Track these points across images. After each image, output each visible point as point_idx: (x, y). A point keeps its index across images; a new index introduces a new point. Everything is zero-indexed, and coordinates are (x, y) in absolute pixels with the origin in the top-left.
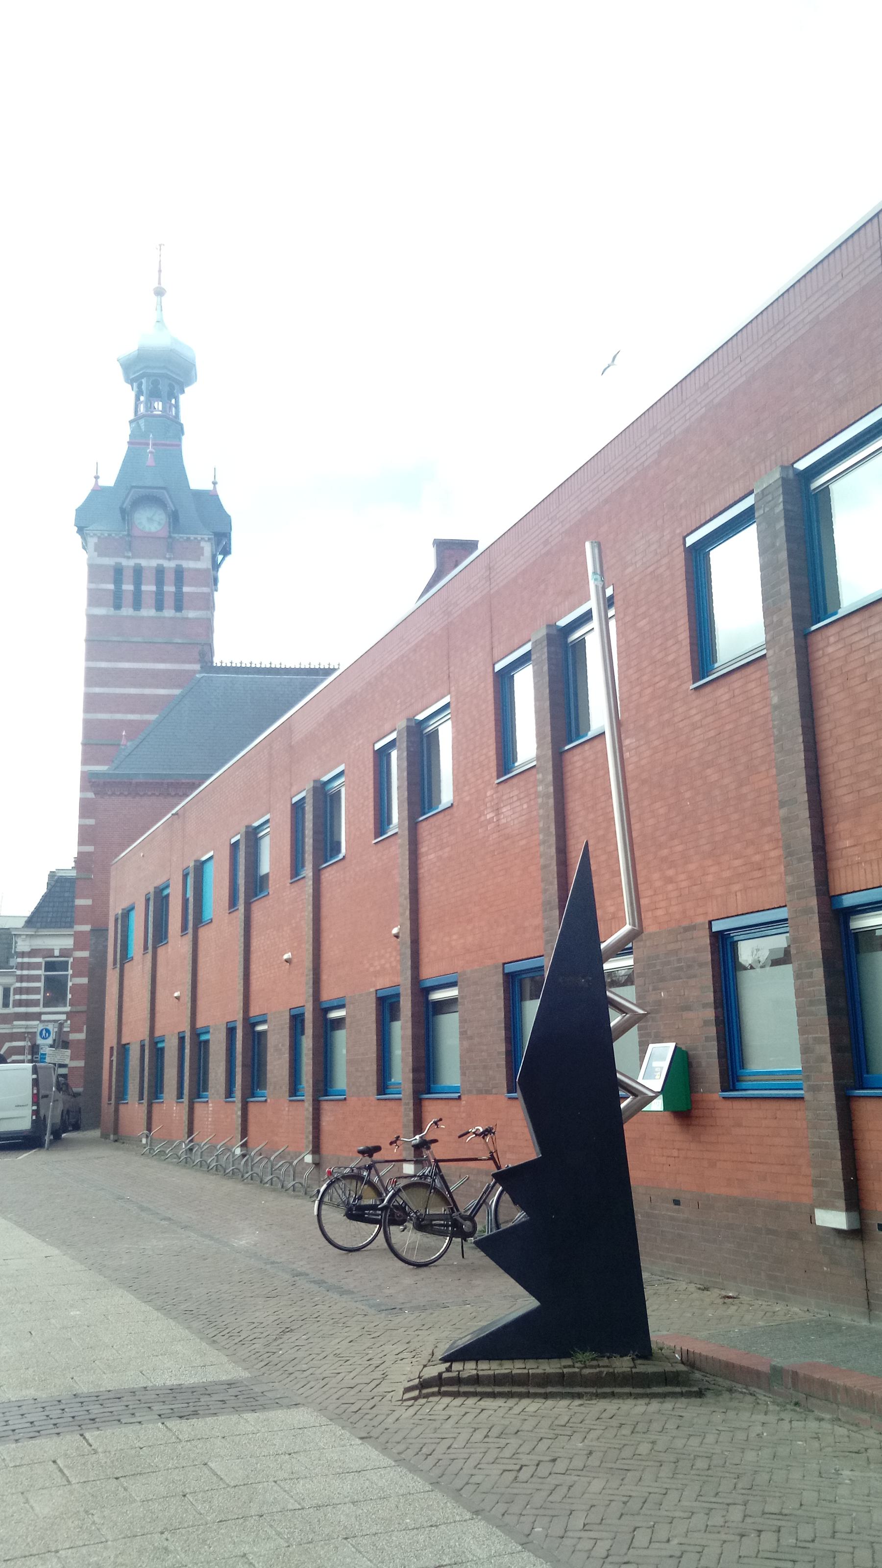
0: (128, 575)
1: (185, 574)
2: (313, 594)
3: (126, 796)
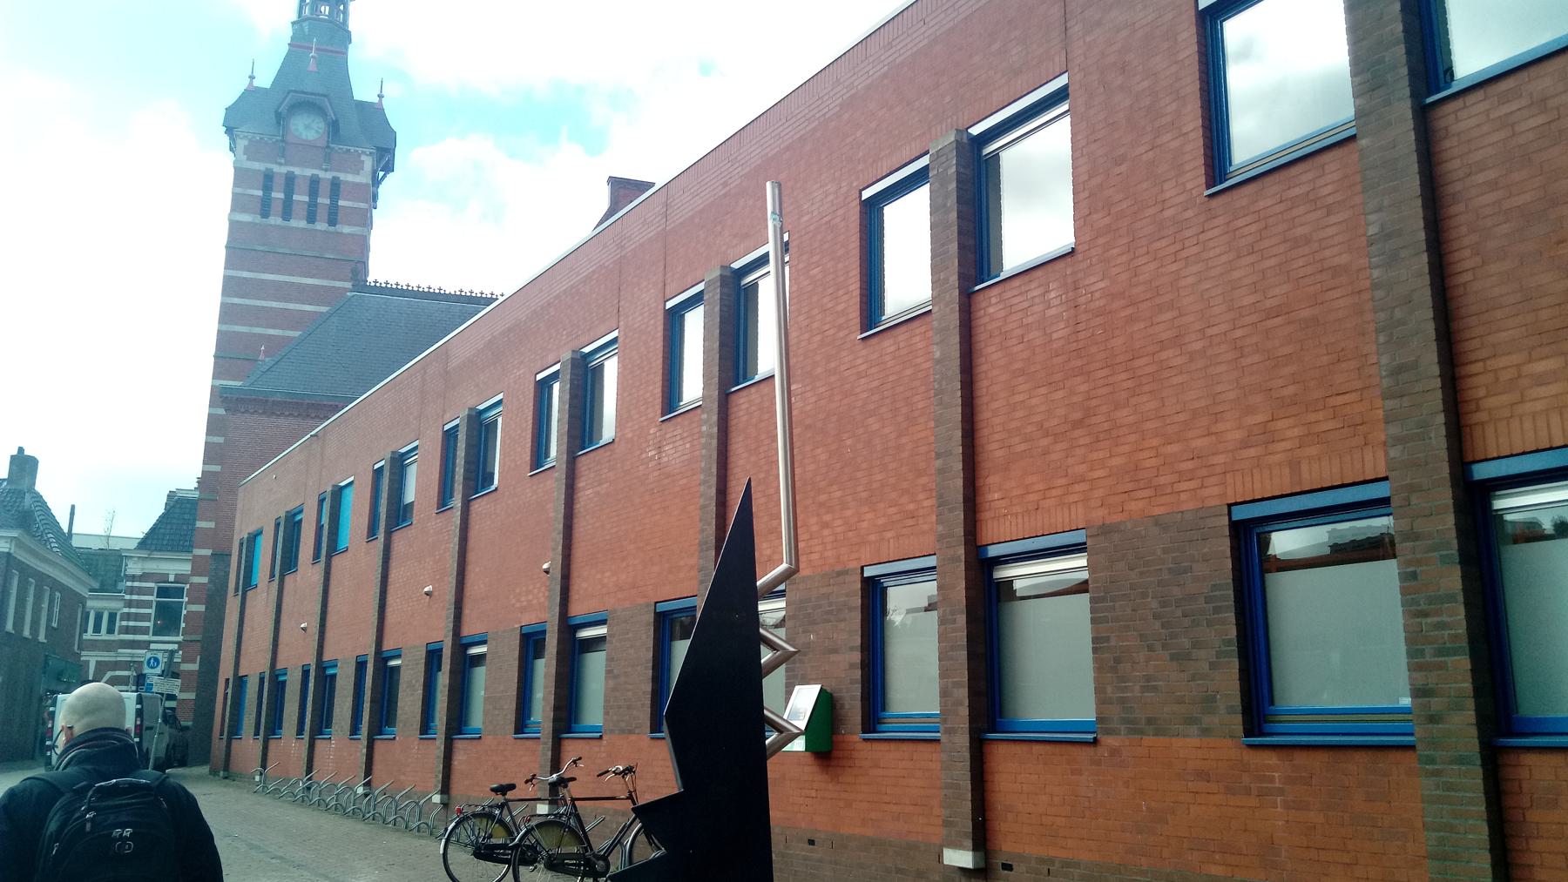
0: (279, 182)
2: (469, 224)
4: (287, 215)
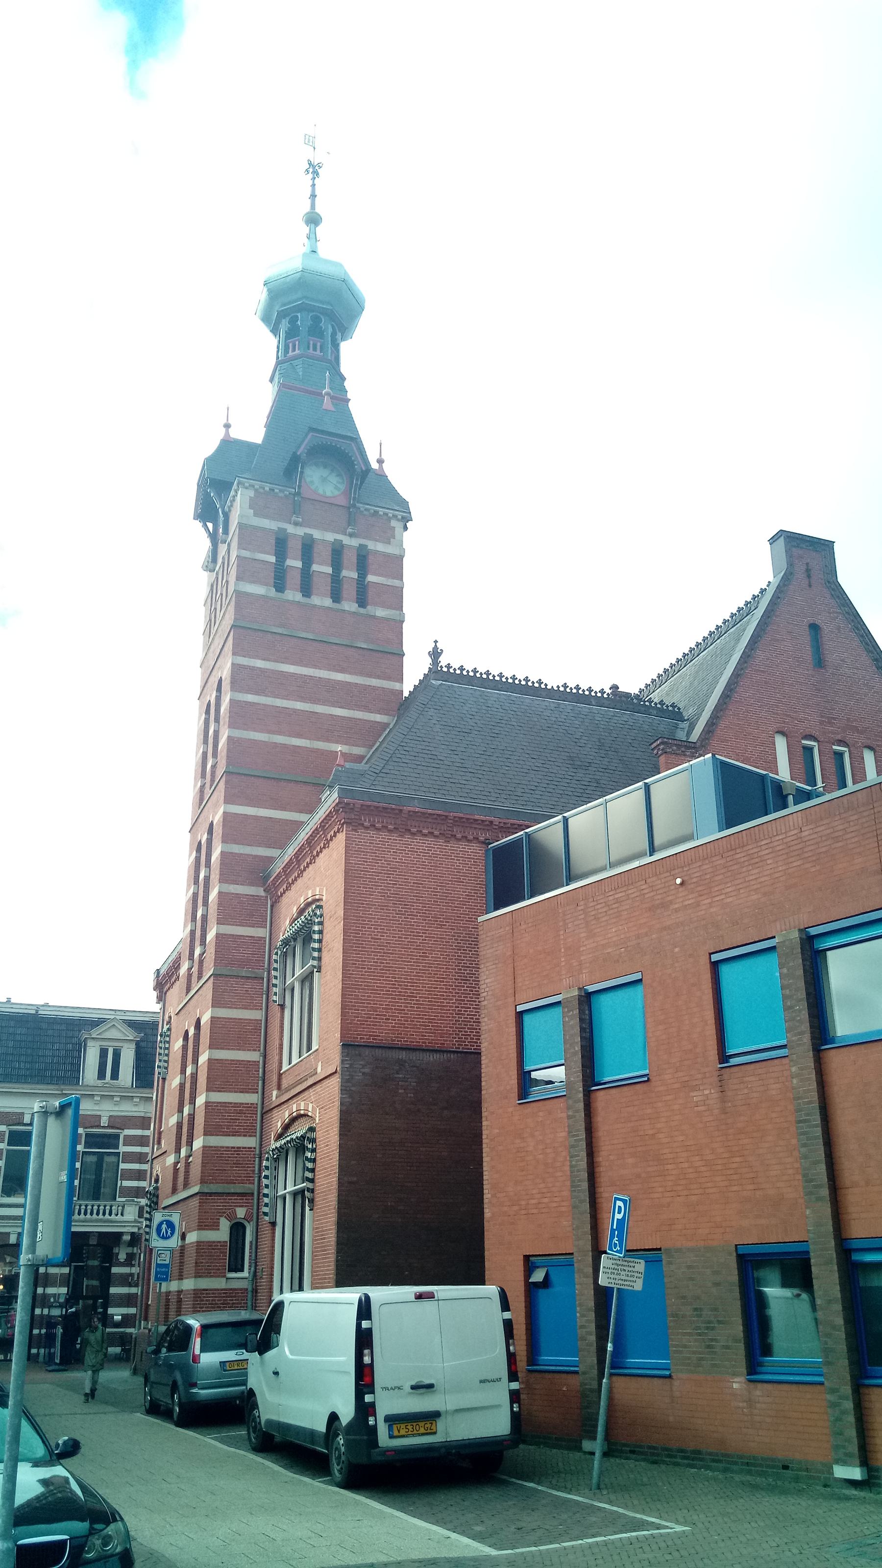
0: (295, 547)
1: (371, 558)
3: (390, 831)
4: (306, 590)
